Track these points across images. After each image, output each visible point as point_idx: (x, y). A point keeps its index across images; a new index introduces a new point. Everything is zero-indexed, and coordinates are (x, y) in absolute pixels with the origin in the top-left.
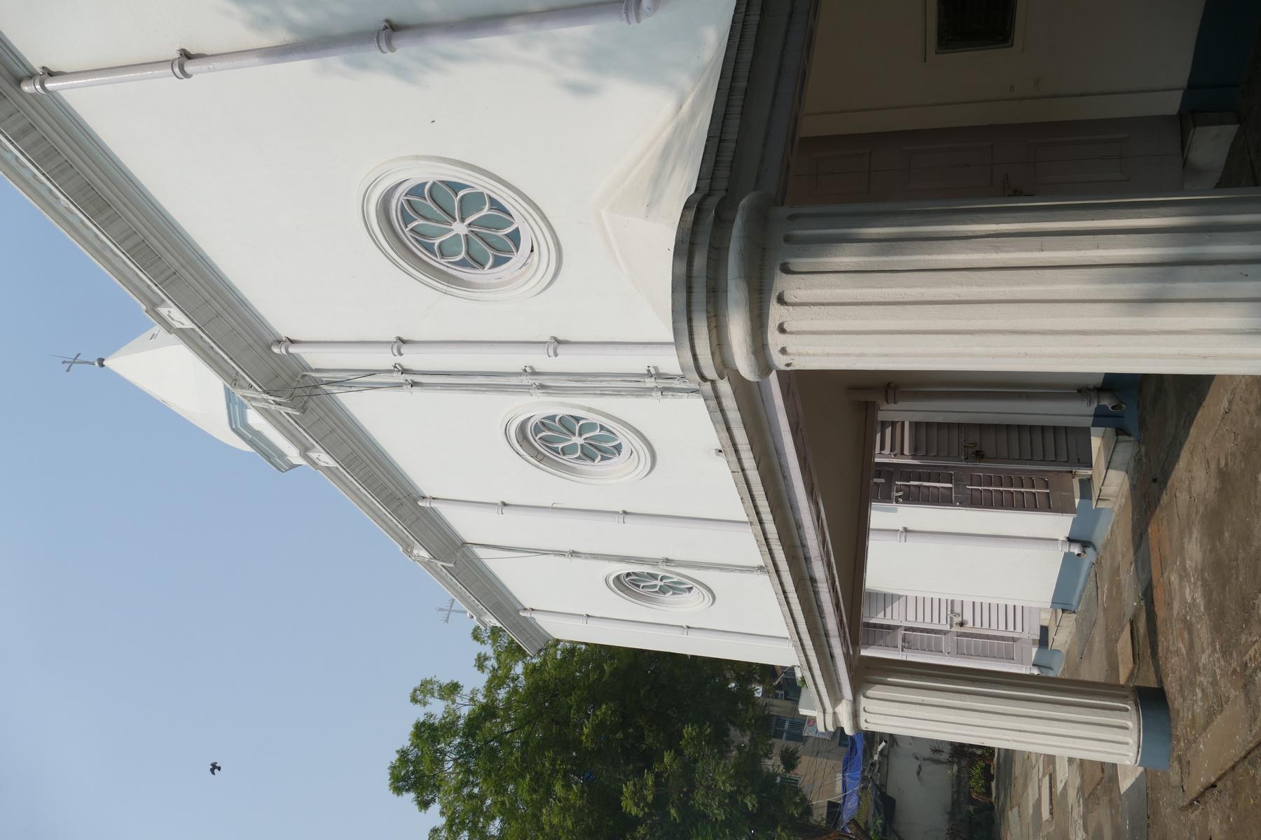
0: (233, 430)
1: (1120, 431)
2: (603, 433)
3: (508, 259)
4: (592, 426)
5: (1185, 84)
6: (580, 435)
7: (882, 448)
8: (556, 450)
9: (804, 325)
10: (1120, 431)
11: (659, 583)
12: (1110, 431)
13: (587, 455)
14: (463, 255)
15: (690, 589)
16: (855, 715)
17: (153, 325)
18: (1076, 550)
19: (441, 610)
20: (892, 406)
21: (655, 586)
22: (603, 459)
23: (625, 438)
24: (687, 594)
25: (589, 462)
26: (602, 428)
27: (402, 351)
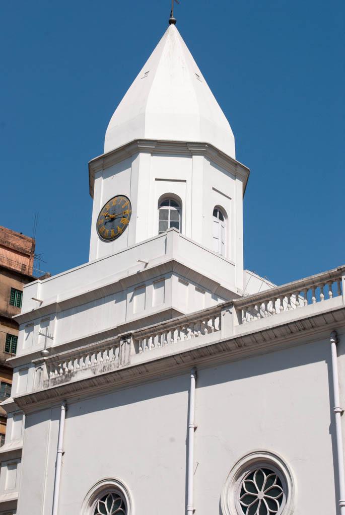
8: (251, 477)
14: (248, 492)
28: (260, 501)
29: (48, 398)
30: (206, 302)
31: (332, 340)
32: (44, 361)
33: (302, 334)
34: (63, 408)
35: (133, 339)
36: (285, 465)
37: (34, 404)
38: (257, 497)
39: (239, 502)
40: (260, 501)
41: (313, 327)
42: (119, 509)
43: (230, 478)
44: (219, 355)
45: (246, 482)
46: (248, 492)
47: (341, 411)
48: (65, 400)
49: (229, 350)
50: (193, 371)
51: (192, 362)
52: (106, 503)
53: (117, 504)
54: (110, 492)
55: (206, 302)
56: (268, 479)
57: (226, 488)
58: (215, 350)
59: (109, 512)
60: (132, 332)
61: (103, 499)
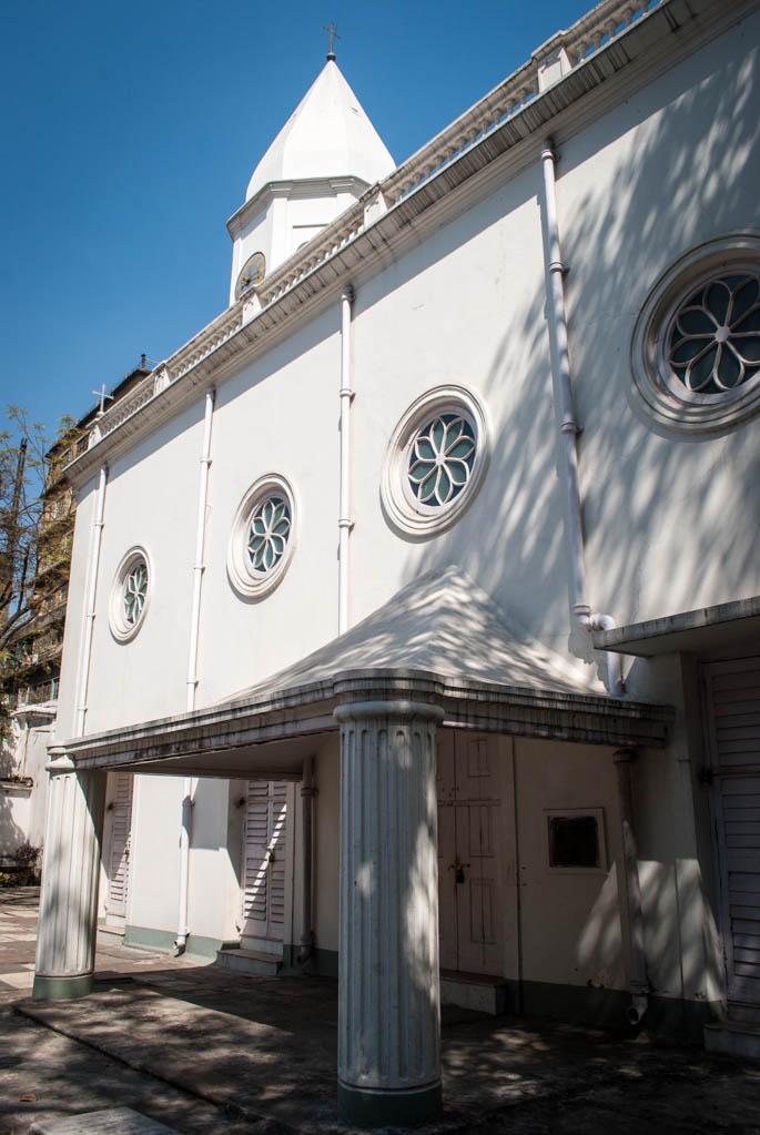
0: (351, 177)
1: (280, 965)
2: (274, 557)
3: (416, 494)
4: (280, 548)
5: (526, 977)
6: (272, 537)
7: (247, 894)
8: (259, 514)
9: (368, 747)
10: (280, 965)
11: (136, 593)
12: (280, 960)
13: (255, 541)
14: (421, 459)
15: (131, 620)
16: (270, 317)
17: (573, 67)
18: (181, 941)
19: (67, 420)
20: (299, 793)
21: (133, 589)
22: (252, 555)
23: (271, 574)
24: (126, 617)
25: (248, 542)
26: (278, 557)
27: (344, 528)
28: (720, 347)
29: (91, 463)
30: (346, 201)
31: (344, 296)
32: (97, 423)
33: (440, 210)
34: (102, 472)
35: (168, 371)
36: (289, 486)
37: (318, 295)
38: (434, 464)
39: (407, 477)
40: (720, 347)
41: (195, 384)
42: (460, 437)
43: (392, 445)
44: (454, 197)
45: (419, 442)
46: (421, 459)
47: (351, 394)
48: (106, 463)
49: (240, 349)
50: (210, 390)
51: (209, 378)
52: (431, 438)
53: (280, 509)
54: (436, 416)
55: (346, 201)
56: (276, 511)
57: (388, 463)
58: (227, 353)
59: (268, 525)
60: (165, 362)
61: (426, 432)
